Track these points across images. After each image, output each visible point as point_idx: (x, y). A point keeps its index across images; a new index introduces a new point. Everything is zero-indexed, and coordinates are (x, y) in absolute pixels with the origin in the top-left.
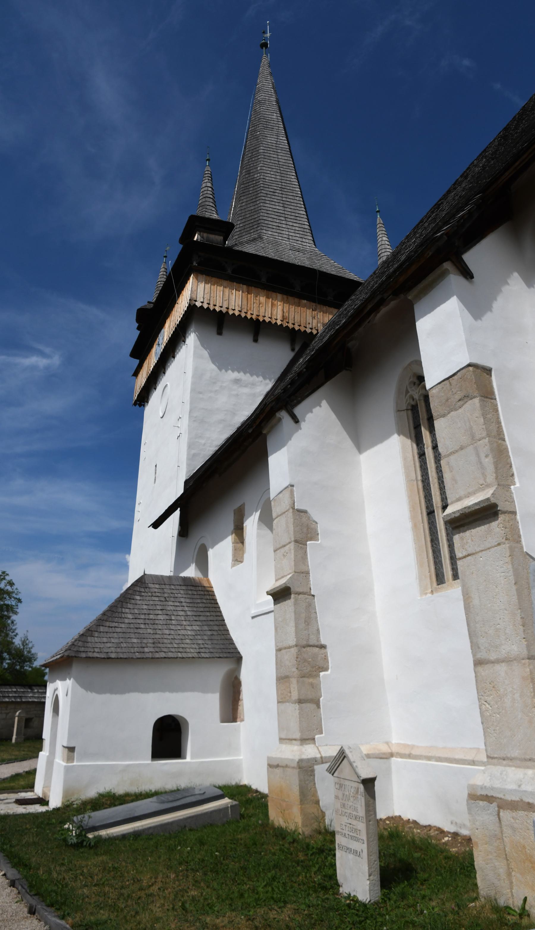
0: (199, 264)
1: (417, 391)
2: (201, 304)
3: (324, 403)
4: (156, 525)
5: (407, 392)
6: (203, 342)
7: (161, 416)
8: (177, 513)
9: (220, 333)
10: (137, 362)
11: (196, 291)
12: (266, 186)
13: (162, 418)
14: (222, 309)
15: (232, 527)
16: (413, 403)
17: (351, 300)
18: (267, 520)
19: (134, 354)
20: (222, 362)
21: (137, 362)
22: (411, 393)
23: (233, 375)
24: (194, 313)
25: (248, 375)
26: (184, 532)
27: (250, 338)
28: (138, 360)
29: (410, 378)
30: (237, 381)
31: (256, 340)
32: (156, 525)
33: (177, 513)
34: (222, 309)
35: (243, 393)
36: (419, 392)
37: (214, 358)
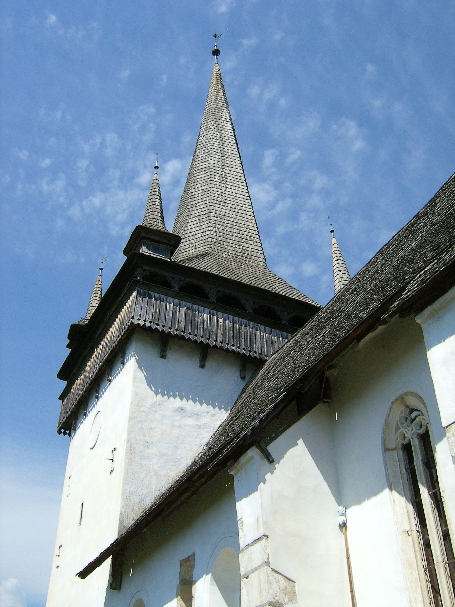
0: (143, 279)
1: (410, 428)
2: (143, 323)
3: (300, 442)
4: (84, 574)
5: (397, 429)
6: (141, 365)
7: (91, 447)
8: (109, 562)
9: (163, 356)
10: (64, 384)
11: (135, 309)
12: (206, 209)
13: (92, 449)
14: (164, 328)
15: (176, 580)
16: (406, 442)
17: (313, 322)
18: (230, 588)
19: (62, 375)
20: (161, 385)
21: (64, 384)
22: (402, 430)
23: (177, 402)
24: (132, 332)
25: (191, 402)
26: (116, 582)
27: (196, 362)
28: (66, 383)
29: (402, 413)
30: (181, 410)
31: (163, 356)
32: (84, 574)
33: (109, 562)
34: (164, 328)
35: (191, 425)
36: (412, 430)
37: (150, 381)
